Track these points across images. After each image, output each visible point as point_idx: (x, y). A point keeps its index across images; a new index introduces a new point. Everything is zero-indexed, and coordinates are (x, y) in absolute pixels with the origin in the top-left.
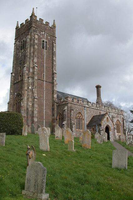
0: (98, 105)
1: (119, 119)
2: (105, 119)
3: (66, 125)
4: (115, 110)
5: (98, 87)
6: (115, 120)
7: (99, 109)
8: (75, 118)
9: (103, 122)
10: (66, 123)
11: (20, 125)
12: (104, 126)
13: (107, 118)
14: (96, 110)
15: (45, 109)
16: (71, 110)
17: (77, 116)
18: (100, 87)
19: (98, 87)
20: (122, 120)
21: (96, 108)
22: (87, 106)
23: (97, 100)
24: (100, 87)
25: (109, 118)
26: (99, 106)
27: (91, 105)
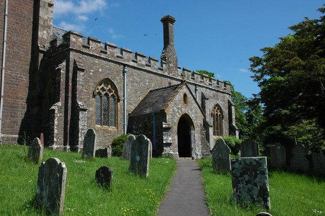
0: (164, 65)
1: (221, 103)
2: (179, 97)
3: (59, 112)
4: (210, 81)
5: (167, 21)
6: (210, 105)
7: (166, 74)
8: (91, 92)
9: (171, 104)
10: (60, 108)
11: (98, 173)
12: (173, 116)
13: (185, 95)
14: (158, 78)
15: (7, 68)
16: (76, 69)
17: (100, 88)
18: (173, 21)
19: (167, 21)
20: (227, 105)
21: (160, 72)
22: (132, 64)
23: (163, 53)
24: (173, 21)
25: (189, 96)
26: (169, 68)
27: (144, 63)
